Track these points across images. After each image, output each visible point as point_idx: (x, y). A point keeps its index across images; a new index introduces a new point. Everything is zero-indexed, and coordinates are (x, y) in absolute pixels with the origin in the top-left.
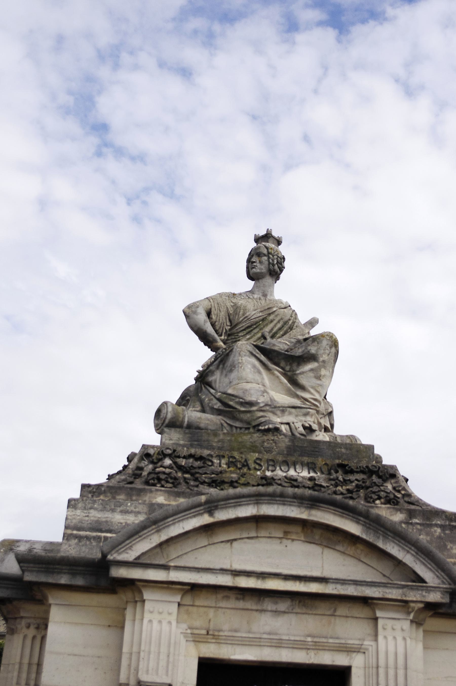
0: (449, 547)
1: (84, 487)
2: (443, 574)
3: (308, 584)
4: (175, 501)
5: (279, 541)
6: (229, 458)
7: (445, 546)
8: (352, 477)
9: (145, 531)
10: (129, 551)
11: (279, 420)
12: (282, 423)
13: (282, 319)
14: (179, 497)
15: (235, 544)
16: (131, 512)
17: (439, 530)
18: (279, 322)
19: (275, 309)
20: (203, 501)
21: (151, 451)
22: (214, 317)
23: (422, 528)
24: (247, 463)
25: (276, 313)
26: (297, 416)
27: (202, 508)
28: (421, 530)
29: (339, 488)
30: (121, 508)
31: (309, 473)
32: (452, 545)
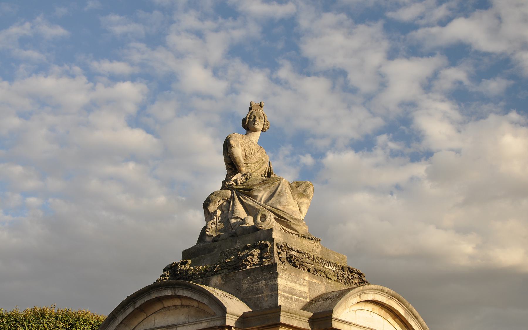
0: (168, 274)
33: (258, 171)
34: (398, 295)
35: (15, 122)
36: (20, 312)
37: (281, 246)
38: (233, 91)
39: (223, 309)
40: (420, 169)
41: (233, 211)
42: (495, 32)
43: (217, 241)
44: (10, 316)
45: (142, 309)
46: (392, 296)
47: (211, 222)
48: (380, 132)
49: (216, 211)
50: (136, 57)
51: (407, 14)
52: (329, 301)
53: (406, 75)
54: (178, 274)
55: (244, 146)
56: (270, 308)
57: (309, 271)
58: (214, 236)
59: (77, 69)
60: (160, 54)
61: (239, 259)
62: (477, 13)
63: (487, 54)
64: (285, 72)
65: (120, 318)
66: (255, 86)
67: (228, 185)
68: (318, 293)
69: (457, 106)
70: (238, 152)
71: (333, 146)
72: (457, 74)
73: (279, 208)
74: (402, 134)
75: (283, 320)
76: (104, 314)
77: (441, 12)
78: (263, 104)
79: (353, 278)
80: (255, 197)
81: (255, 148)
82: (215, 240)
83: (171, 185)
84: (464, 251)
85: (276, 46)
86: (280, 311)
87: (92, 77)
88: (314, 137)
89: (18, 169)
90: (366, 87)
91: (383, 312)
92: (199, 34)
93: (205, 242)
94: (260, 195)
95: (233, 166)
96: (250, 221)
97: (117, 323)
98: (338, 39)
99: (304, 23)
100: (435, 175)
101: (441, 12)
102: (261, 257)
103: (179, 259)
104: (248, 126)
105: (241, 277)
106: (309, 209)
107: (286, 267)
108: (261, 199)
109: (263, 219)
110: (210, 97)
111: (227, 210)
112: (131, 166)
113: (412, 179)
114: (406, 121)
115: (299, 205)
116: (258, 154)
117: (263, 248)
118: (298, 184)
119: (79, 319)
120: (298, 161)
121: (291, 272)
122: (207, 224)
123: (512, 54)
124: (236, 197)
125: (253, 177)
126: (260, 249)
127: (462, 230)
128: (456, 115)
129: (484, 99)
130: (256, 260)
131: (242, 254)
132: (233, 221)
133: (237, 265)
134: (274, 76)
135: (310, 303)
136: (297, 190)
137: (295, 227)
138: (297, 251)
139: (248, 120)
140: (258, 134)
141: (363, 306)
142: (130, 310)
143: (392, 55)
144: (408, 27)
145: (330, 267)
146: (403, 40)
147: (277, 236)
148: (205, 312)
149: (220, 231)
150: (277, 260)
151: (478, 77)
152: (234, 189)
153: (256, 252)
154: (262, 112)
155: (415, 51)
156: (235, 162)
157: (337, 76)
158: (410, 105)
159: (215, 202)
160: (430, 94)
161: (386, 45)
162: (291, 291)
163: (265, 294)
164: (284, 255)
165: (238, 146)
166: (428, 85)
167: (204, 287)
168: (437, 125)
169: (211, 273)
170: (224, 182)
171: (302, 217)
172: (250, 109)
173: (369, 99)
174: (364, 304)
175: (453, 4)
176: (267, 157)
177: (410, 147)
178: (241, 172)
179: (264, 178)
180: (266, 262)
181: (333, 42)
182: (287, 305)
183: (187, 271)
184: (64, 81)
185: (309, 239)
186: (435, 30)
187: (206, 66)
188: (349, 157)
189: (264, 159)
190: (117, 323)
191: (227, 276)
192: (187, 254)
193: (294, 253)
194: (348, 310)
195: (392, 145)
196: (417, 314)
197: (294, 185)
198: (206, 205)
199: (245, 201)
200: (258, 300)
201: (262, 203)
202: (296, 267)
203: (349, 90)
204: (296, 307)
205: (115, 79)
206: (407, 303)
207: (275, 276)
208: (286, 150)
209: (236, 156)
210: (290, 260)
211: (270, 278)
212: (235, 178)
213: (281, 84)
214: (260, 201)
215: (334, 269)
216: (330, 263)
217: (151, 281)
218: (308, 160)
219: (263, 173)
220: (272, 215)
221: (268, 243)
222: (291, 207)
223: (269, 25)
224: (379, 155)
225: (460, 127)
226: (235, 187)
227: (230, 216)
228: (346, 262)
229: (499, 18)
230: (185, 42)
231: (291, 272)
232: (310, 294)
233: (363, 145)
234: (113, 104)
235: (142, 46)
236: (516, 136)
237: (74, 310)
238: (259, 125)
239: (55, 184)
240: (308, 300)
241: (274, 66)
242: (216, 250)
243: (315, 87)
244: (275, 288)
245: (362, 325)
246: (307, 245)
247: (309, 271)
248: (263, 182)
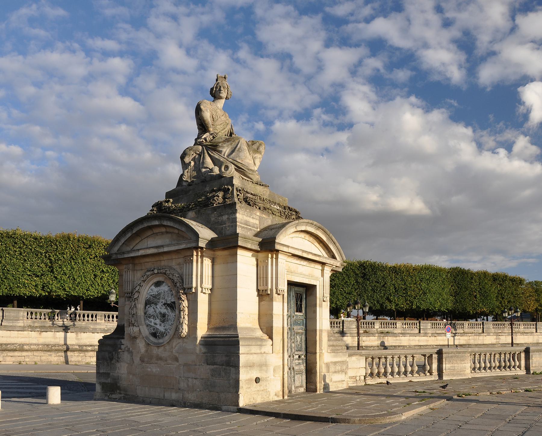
0: (155, 209)
33: (223, 132)
34: (323, 227)
35: (31, 90)
36: (53, 235)
37: (240, 190)
38: (202, 68)
39: (196, 235)
40: (343, 137)
41: (203, 163)
42: (405, 31)
43: (191, 185)
44: (46, 238)
45: (138, 234)
46: (319, 228)
47: (186, 171)
48: (316, 107)
49: (190, 162)
50: (123, 36)
51: (341, 10)
52: (274, 230)
53: (338, 60)
54: (163, 210)
55: (213, 111)
56: (231, 235)
57: (260, 208)
58: (189, 181)
59: (76, 46)
60: (142, 34)
61: (208, 199)
62: (393, 14)
63: (398, 49)
64: (243, 54)
65: (123, 241)
66: (221, 62)
67: (199, 142)
68: (266, 225)
69: (374, 89)
70: (207, 115)
71: (280, 116)
72: (375, 63)
73: (239, 161)
74: (331, 109)
75: (240, 243)
76: (110, 238)
77: (367, 11)
78: (227, 76)
79: (292, 214)
80: (220, 152)
81: (220, 112)
82: (190, 185)
83: (154, 143)
84: (370, 199)
85: (237, 31)
86: (238, 237)
87: (89, 52)
88: (266, 108)
89: (37, 129)
90: (307, 69)
91: (311, 239)
92: (174, 18)
93: (182, 186)
94: (224, 150)
95: (203, 127)
96: (216, 171)
97: (120, 244)
98: (286, 27)
99: (259, 11)
100: (355, 142)
101: (367, 11)
102: (224, 198)
103: (163, 198)
104: (215, 94)
105: (210, 212)
106: (261, 163)
107: (243, 205)
108: (225, 153)
109: (226, 169)
110: (183, 72)
111: (199, 162)
112: (123, 127)
113: (338, 144)
114: (336, 98)
115: (254, 159)
116: (223, 117)
117: (226, 191)
118: (253, 143)
119: (94, 241)
120: (253, 127)
121: (246, 209)
122: (184, 172)
123: (416, 51)
124: (205, 151)
125: (218, 136)
126: (224, 191)
127: (370, 184)
128: (373, 96)
129: (394, 85)
130: (220, 200)
131: (211, 195)
132: (204, 170)
133: (207, 203)
134: (235, 57)
135: (260, 231)
136: (252, 148)
137: (250, 176)
138: (252, 194)
139: (215, 89)
140: (223, 101)
141: (297, 235)
142: (129, 235)
143: (328, 44)
144: (341, 22)
145: (275, 207)
146: (337, 32)
147: (237, 182)
148: (183, 237)
149: (194, 177)
150: (236, 200)
151: (391, 66)
152: (204, 145)
153: (221, 194)
154: (226, 83)
155: (345, 42)
156: (205, 123)
157: (284, 58)
158: (340, 86)
159: (190, 155)
160: (355, 78)
161: (323, 34)
162: (247, 223)
163: (227, 225)
164: (241, 196)
165: (207, 110)
166: (354, 70)
167: (182, 219)
168: (358, 103)
169: (188, 209)
170: (196, 140)
171: (256, 168)
172: (217, 80)
173: (309, 78)
174: (298, 233)
175: (376, 5)
176: (230, 121)
177: (338, 119)
178: (209, 131)
179: (227, 137)
180: (228, 202)
181: (283, 30)
182: (244, 233)
183: (169, 208)
184: (67, 57)
185: (260, 185)
186: (362, 25)
187: (180, 46)
188: (292, 125)
189: (227, 122)
190: (120, 244)
191: (199, 211)
192: (169, 195)
193: (249, 195)
194: (287, 237)
195: (325, 117)
196: (335, 241)
197: (250, 143)
198: (183, 157)
199: (212, 154)
200: (222, 229)
201: (225, 156)
202: (251, 205)
203: (294, 70)
204: (250, 234)
205: (107, 54)
206: (329, 232)
207: (235, 211)
208: (243, 118)
209: (205, 119)
210: (246, 200)
211: (231, 213)
212: (204, 136)
213: (241, 64)
214: (224, 155)
215: (278, 208)
216: (275, 203)
217: (144, 214)
218: (260, 126)
219: (226, 133)
220: (233, 166)
221: (230, 187)
222: (247, 161)
223: (231, 12)
224: (315, 124)
225: (375, 105)
226: (205, 144)
227: (201, 166)
228: (287, 204)
229: (409, 20)
230: (163, 25)
231: (246, 209)
232: (260, 225)
233: (303, 116)
234: (106, 75)
235: (127, 26)
236: (413, 114)
237: (90, 235)
238: (224, 94)
239: (66, 141)
240: (259, 230)
241: (235, 48)
242: (191, 192)
243: (267, 67)
244: (234, 221)
245: (296, 247)
246: (259, 190)
247: (260, 208)
248: (227, 140)
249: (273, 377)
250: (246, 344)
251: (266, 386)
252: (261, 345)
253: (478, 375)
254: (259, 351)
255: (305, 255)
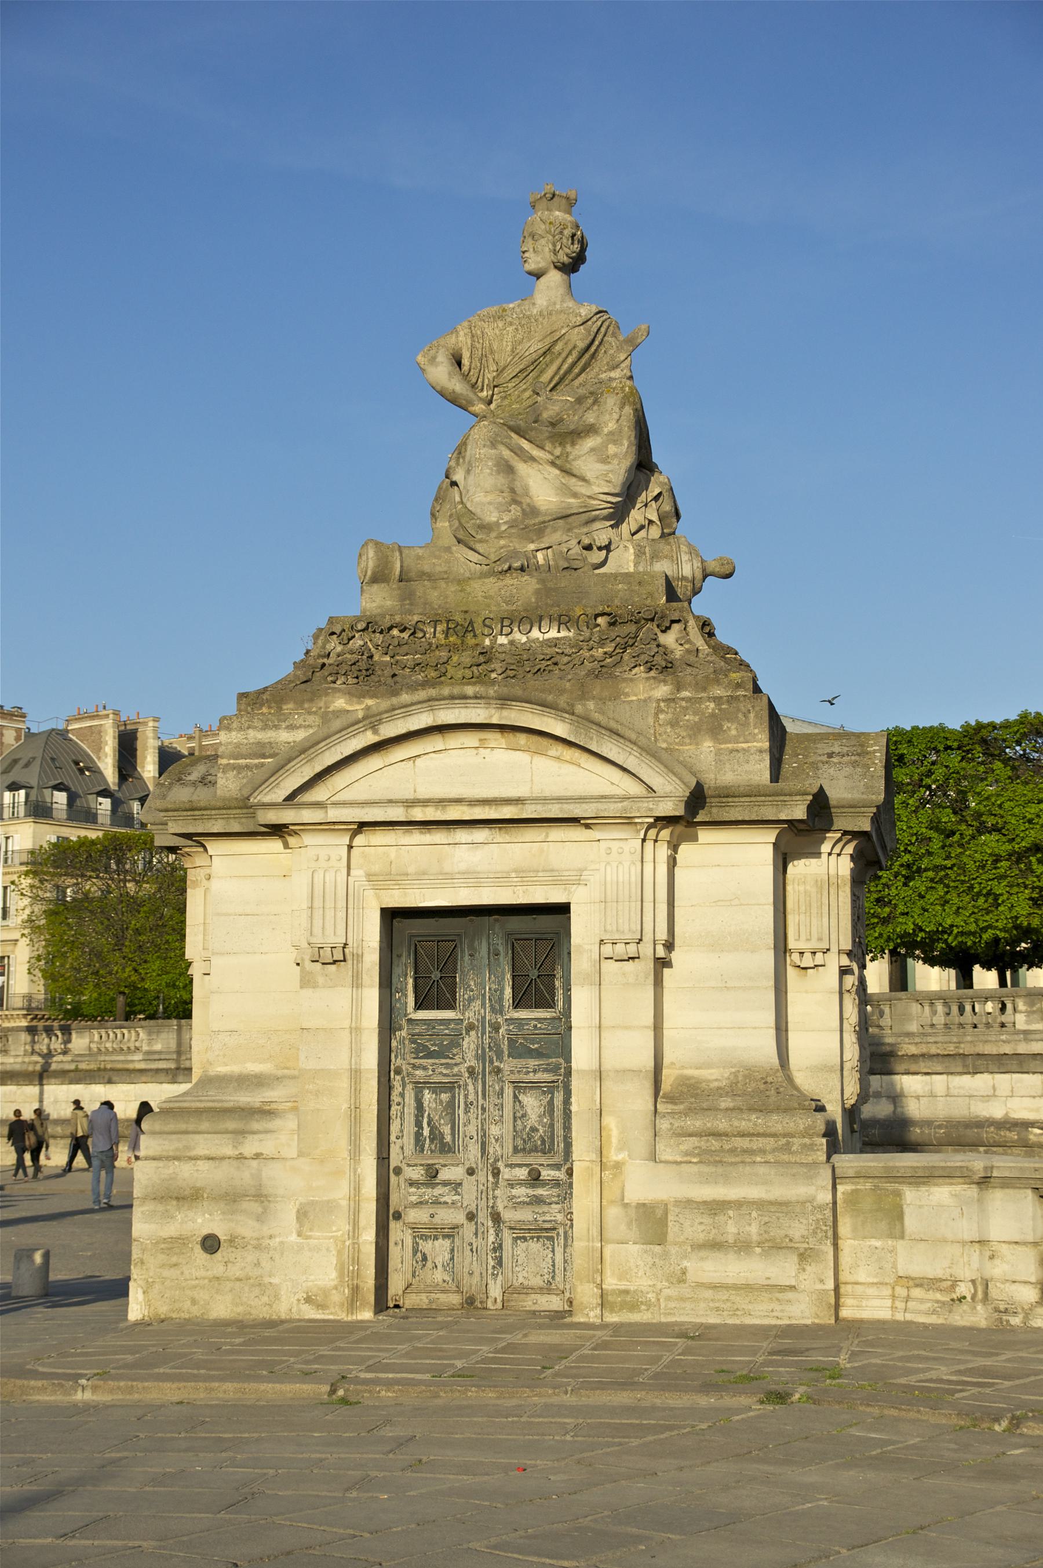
0: (725, 728)
1: (242, 696)
2: (674, 778)
3: (500, 808)
4: (359, 703)
5: (474, 751)
6: (448, 621)
7: (721, 726)
8: (617, 630)
9: (292, 764)
10: (276, 790)
11: (532, 547)
12: (537, 551)
13: (574, 347)
14: (364, 697)
15: (418, 760)
16: (300, 726)
17: (712, 705)
18: (570, 353)
19: (563, 331)
20: (360, 717)
21: (337, 629)
22: (466, 361)
23: (689, 704)
24: (473, 627)
25: (566, 337)
26: (569, 530)
27: (361, 725)
28: (687, 708)
29: (594, 652)
30: (287, 723)
31: (559, 632)
32: (729, 725)
249: (293, 1238)
250: (171, 1127)
251: (258, 1264)
252: (242, 1133)
253: (612, 1318)
254: (229, 1151)
255: (418, 814)
